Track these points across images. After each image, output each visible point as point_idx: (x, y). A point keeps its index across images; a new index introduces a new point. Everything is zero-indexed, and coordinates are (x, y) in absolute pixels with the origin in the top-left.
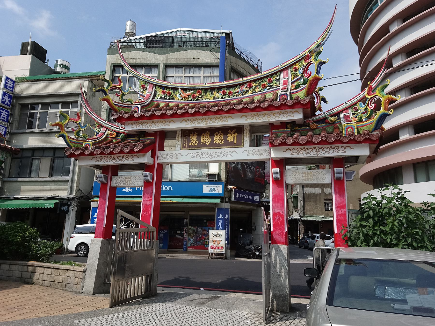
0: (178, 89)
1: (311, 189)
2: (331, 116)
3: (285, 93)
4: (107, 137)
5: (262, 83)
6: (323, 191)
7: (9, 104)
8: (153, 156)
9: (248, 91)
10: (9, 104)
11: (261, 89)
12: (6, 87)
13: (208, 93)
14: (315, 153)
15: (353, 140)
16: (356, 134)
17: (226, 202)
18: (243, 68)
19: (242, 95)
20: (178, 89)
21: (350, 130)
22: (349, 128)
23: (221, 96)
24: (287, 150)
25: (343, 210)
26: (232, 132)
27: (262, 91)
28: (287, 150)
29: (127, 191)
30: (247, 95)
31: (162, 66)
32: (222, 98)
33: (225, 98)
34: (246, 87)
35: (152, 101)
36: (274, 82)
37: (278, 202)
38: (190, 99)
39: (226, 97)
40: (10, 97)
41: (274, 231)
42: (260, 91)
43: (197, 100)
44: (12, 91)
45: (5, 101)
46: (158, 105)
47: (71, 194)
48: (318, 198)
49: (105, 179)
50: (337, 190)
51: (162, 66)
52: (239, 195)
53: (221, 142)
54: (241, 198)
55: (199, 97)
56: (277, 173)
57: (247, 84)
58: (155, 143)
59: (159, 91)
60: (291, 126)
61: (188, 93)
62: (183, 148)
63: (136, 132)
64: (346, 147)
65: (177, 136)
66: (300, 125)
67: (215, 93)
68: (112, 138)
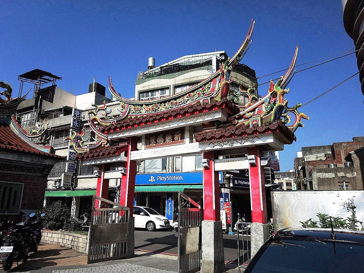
0: (143, 105)
1: (324, 174)
2: (248, 113)
3: (206, 98)
4: (101, 144)
5: (198, 92)
6: (336, 175)
7: (78, 127)
8: (126, 155)
9: (188, 100)
10: (78, 127)
11: (197, 97)
12: (75, 115)
13: (163, 105)
14: (231, 144)
15: (256, 132)
16: (260, 125)
17: (226, 188)
18: (236, 78)
19: (185, 103)
20: (143, 105)
21: (255, 122)
22: (254, 121)
23: (170, 106)
24: (210, 143)
25: (257, 191)
26: (177, 133)
27: (198, 99)
28: (210, 143)
29: (152, 181)
30: (188, 103)
31: (172, 87)
32: (171, 108)
33: (173, 107)
34: (187, 97)
35: (127, 115)
36: (207, 90)
37: (208, 186)
38: (150, 111)
39: (174, 106)
40: (78, 122)
41: (205, 209)
42: (197, 99)
43: (155, 111)
44: (80, 118)
45: (75, 125)
46: (131, 118)
47: (117, 185)
48: (332, 181)
49: (99, 174)
50: (253, 175)
51: (172, 87)
52: (238, 182)
53: (170, 141)
54: (239, 185)
55: (156, 109)
56: (205, 163)
57: (188, 95)
58: (128, 146)
59: (133, 107)
60: (217, 124)
61: (150, 107)
62: (146, 148)
63: (127, 137)
64: (254, 137)
65: (186, 137)
66: (224, 123)
67: (166, 104)
68: (104, 145)
